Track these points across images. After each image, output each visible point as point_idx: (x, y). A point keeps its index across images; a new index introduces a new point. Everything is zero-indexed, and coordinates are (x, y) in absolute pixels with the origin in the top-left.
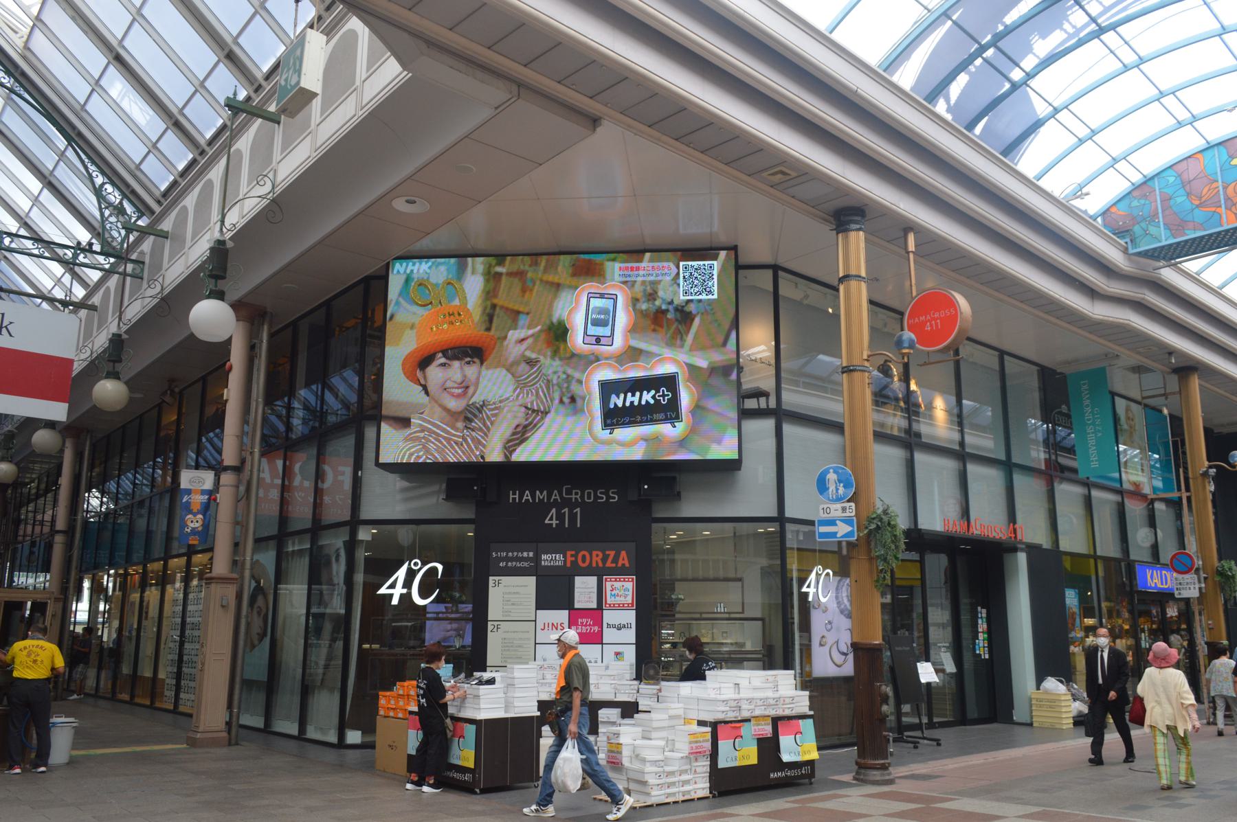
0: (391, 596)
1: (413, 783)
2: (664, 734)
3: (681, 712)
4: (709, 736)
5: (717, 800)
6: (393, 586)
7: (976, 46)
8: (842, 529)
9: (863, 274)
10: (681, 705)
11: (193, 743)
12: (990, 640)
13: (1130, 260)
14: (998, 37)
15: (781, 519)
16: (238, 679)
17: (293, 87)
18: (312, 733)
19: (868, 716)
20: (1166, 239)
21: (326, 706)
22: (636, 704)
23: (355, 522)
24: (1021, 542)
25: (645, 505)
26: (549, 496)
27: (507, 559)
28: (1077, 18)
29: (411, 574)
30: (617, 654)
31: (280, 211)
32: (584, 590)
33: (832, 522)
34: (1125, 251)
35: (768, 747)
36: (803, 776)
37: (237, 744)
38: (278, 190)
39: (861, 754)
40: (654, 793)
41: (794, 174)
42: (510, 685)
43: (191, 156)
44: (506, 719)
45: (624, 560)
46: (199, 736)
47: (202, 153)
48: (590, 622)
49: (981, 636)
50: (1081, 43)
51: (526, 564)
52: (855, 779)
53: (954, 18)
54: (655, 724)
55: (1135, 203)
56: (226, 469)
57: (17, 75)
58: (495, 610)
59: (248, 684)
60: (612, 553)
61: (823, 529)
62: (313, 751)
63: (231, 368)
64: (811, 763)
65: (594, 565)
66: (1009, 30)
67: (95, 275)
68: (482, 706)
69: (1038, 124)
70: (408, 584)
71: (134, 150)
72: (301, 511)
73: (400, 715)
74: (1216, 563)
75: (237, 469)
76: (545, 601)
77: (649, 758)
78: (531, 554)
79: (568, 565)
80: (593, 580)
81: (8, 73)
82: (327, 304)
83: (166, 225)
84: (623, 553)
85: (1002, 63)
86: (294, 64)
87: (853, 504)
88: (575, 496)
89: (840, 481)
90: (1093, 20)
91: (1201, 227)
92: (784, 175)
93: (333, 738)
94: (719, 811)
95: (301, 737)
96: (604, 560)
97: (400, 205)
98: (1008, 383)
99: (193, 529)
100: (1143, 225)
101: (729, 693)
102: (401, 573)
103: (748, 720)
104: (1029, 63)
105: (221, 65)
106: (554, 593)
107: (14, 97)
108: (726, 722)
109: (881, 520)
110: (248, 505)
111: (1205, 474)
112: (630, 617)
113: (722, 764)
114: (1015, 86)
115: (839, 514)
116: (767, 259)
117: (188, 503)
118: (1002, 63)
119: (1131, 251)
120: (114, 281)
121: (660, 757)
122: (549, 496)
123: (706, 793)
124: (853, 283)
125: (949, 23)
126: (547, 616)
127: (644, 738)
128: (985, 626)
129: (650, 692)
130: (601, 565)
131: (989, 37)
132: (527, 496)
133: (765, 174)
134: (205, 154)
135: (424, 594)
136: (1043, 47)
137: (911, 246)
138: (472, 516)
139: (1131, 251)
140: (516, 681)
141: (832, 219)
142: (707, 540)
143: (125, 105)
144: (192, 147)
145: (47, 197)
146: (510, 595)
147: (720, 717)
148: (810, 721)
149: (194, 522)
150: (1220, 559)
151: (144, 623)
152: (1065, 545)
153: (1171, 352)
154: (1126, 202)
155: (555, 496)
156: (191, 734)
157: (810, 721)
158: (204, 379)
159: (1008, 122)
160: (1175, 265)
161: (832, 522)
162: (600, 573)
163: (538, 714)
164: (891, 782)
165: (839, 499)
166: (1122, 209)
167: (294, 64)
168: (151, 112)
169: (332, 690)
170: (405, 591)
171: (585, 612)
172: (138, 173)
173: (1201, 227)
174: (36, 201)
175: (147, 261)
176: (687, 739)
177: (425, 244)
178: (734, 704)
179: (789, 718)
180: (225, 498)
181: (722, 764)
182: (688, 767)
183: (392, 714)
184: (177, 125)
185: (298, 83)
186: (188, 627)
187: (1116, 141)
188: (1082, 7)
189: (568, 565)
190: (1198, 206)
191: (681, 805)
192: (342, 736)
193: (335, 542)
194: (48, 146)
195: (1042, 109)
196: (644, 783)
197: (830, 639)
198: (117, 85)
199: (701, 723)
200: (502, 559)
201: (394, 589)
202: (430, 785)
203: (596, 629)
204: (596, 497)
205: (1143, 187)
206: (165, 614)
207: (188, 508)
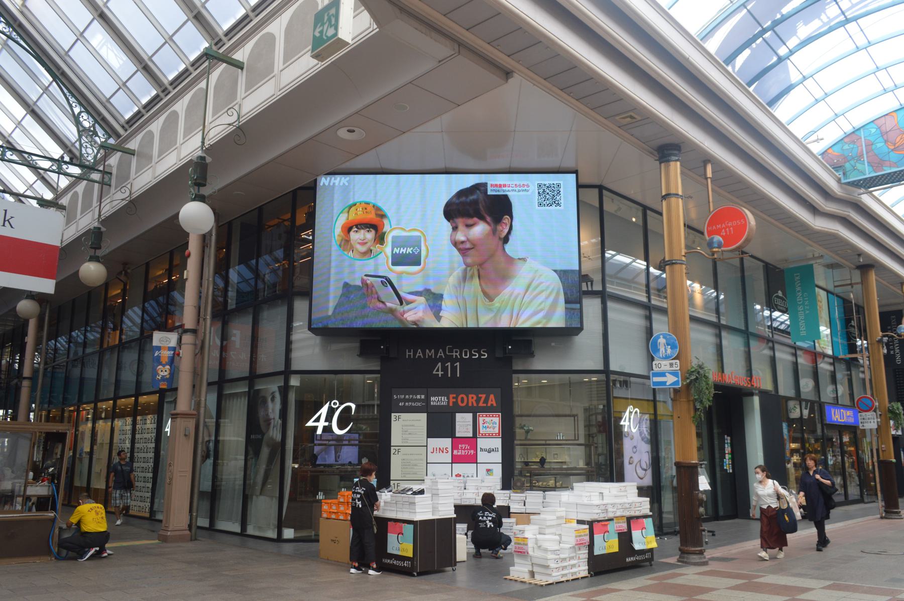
0: (316, 428)
1: (355, 568)
2: (553, 530)
3: (563, 514)
4: (587, 532)
5: (595, 579)
6: (318, 420)
7: (760, 29)
8: (670, 379)
9: (680, 193)
10: (564, 509)
11: (164, 539)
12: (733, 459)
13: (841, 188)
14: (776, 23)
15: (606, 370)
16: (196, 491)
17: (329, 38)
18: (250, 531)
19: (697, 512)
20: (869, 173)
21: (264, 508)
22: (509, 507)
23: (287, 372)
24: (756, 388)
25: (507, 361)
26: (436, 354)
27: (405, 400)
28: (832, 11)
29: (331, 411)
30: (488, 470)
31: (243, 136)
32: (463, 423)
33: (663, 374)
34: (839, 181)
35: (625, 538)
36: (646, 560)
37: (196, 539)
38: (243, 120)
39: (684, 542)
40: (554, 574)
41: (639, 118)
42: (435, 495)
43: (154, 93)
44: (434, 520)
45: (492, 401)
46: (169, 533)
47: (165, 91)
48: (467, 447)
49: (727, 456)
50: (831, 30)
51: (419, 404)
52: (679, 561)
53: (749, 8)
54: (548, 523)
55: (846, 147)
56: (186, 331)
57: (15, 26)
58: (396, 438)
59: (202, 494)
60: (484, 396)
61: (656, 379)
62: (251, 542)
63: (189, 255)
64: (651, 550)
65: (470, 405)
66: (784, 19)
67: (64, 182)
68: (417, 510)
69: (790, 88)
70: (329, 418)
71: (104, 85)
72: (239, 365)
73: (341, 517)
74: (888, 405)
75: (194, 331)
76: (433, 432)
77: (550, 548)
78: (423, 397)
79: (451, 404)
80: (469, 416)
81: (8, 24)
82: (260, 209)
83: (133, 145)
84: (492, 396)
85: (775, 42)
86: (329, 20)
87: (678, 361)
88: (455, 354)
89: (668, 345)
90: (843, 13)
91: (895, 165)
92: (630, 117)
93: (273, 534)
94: (604, 587)
95: (243, 534)
96: (478, 401)
97: (343, 133)
98: (746, 274)
99: (163, 376)
100: (852, 162)
101: (596, 500)
102: (324, 411)
103: (611, 520)
104: (792, 43)
105: (95, 21)
106: (441, 425)
107: (10, 42)
108: (599, 521)
109: (698, 373)
110: (203, 359)
111: (880, 341)
112: (497, 443)
113: (597, 552)
114: (780, 60)
115: (668, 368)
116: (596, 182)
117: (159, 357)
118: (775, 42)
119: (843, 181)
120: (81, 188)
121: (557, 548)
122: (436, 354)
123: (585, 573)
124: (673, 200)
125: (745, 11)
126: (435, 442)
127: (540, 533)
128: (730, 449)
129: (518, 498)
130: (475, 405)
131: (769, 23)
132: (419, 353)
133: (617, 118)
134: (166, 92)
135: (341, 427)
136: (804, 31)
137: (709, 174)
138: (378, 368)
139: (843, 181)
140: (440, 492)
141: (656, 153)
142: (542, 387)
143: (103, 52)
144: (156, 85)
145: (30, 123)
146: (408, 427)
147: (596, 517)
148: (650, 520)
149: (163, 372)
150: (890, 402)
151: (95, 447)
152: (782, 392)
153: (860, 253)
154: (839, 146)
155: (441, 353)
156: (161, 533)
157: (650, 520)
158: (147, 264)
159: (772, 84)
160: (871, 192)
161: (663, 374)
162: (475, 411)
163: (455, 516)
164: (705, 564)
165: (666, 358)
166: (837, 150)
167: (329, 20)
168: (125, 58)
169: (272, 497)
170: (327, 424)
171: (464, 439)
172: (108, 105)
173: (895, 165)
174: (19, 124)
175: (114, 171)
176: (574, 534)
177: (358, 163)
178: (603, 508)
179: (638, 517)
180: (186, 353)
181: (597, 552)
182: (574, 555)
183: (333, 516)
184: (146, 68)
185: (336, 34)
186: (136, 450)
187: (838, 102)
188: (837, 3)
189: (451, 404)
190: (892, 150)
191: (580, 582)
192: (280, 533)
193: (273, 387)
194: (35, 80)
195: (795, 77)
196: (547, 567)
197: (636, 460)
198: (99, 37)
199: (580, 522)
200: (401, 400)
201: (319, 422)
202: (374, 569)
203: (472, 452)
204: (471, 355)
205: (852, 136)
206: (115, 441)
207: (158, 361)
